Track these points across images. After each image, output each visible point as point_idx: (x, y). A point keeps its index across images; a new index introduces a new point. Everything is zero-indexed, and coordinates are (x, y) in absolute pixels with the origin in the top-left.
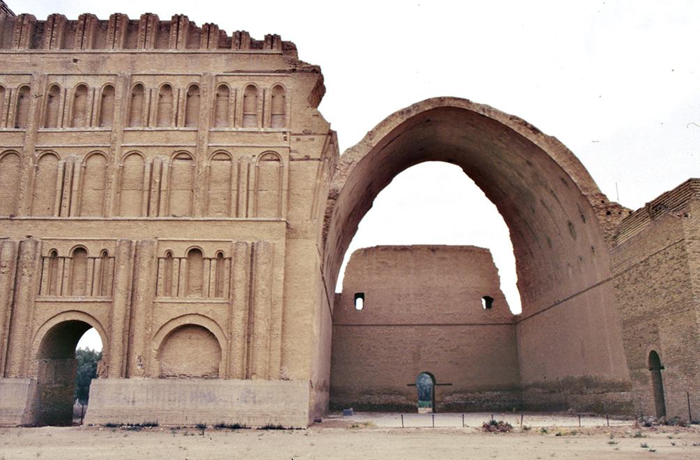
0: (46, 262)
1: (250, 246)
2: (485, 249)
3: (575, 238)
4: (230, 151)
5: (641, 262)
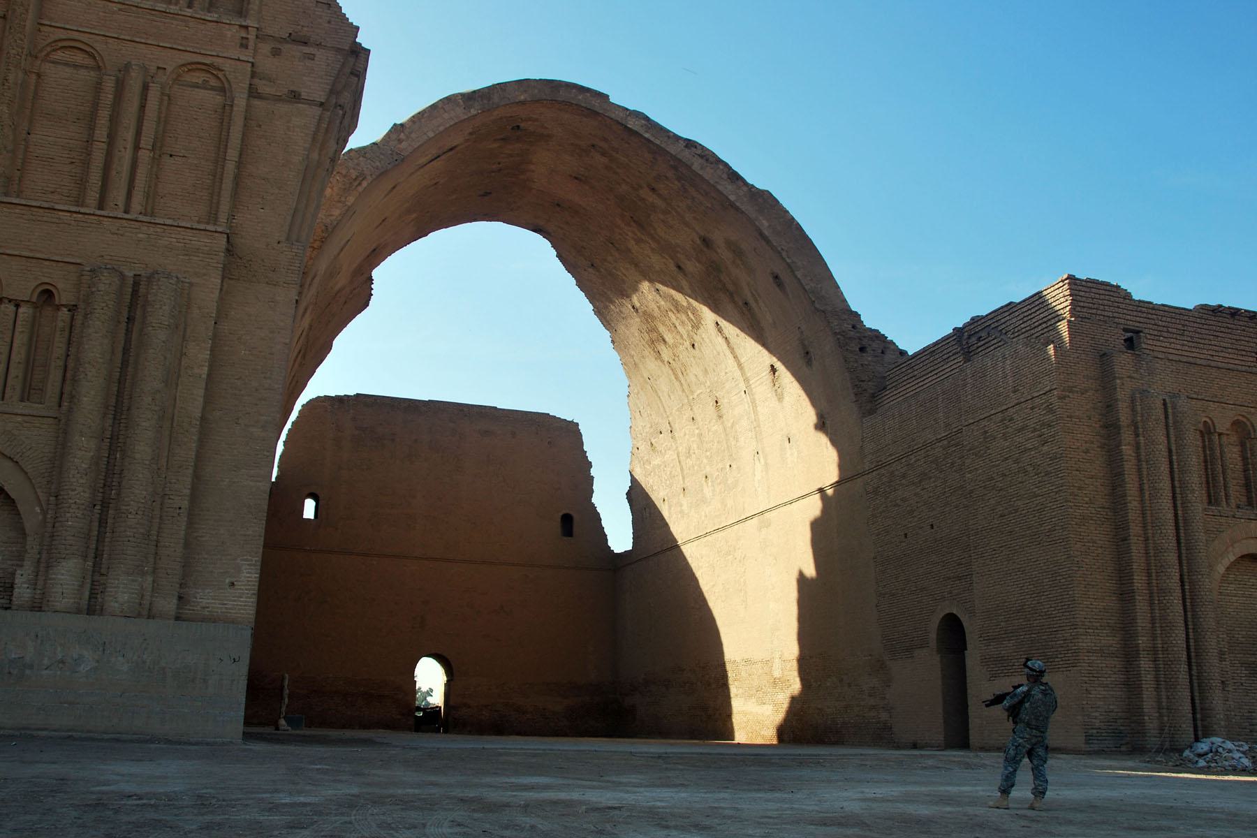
1: (131, 281)
3: (780, 398)
4: (98, 46)
5: (939, 440)
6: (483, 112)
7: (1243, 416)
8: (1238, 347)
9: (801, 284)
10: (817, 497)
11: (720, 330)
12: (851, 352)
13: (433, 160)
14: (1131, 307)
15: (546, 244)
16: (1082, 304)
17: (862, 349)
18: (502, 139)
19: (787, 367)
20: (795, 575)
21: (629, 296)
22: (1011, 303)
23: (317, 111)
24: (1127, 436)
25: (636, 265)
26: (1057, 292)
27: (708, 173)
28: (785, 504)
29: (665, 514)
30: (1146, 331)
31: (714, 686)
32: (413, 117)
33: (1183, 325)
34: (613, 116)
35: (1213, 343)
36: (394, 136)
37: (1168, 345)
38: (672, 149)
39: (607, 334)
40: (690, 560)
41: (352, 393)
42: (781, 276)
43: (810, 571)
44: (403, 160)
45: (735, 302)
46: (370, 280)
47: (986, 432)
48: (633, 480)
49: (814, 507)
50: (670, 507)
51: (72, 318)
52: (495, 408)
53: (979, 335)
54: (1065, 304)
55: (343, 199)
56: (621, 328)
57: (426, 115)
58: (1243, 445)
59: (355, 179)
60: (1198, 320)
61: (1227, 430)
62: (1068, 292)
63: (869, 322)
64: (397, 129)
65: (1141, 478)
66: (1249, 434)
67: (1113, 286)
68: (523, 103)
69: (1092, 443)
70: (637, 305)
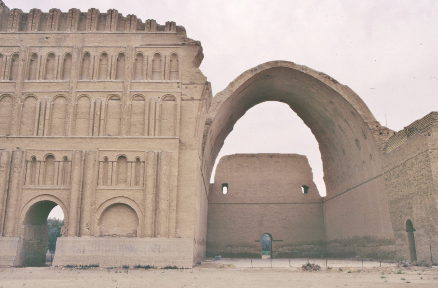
0: (29, 164)
4: (144, 94)
51: (144, 165)
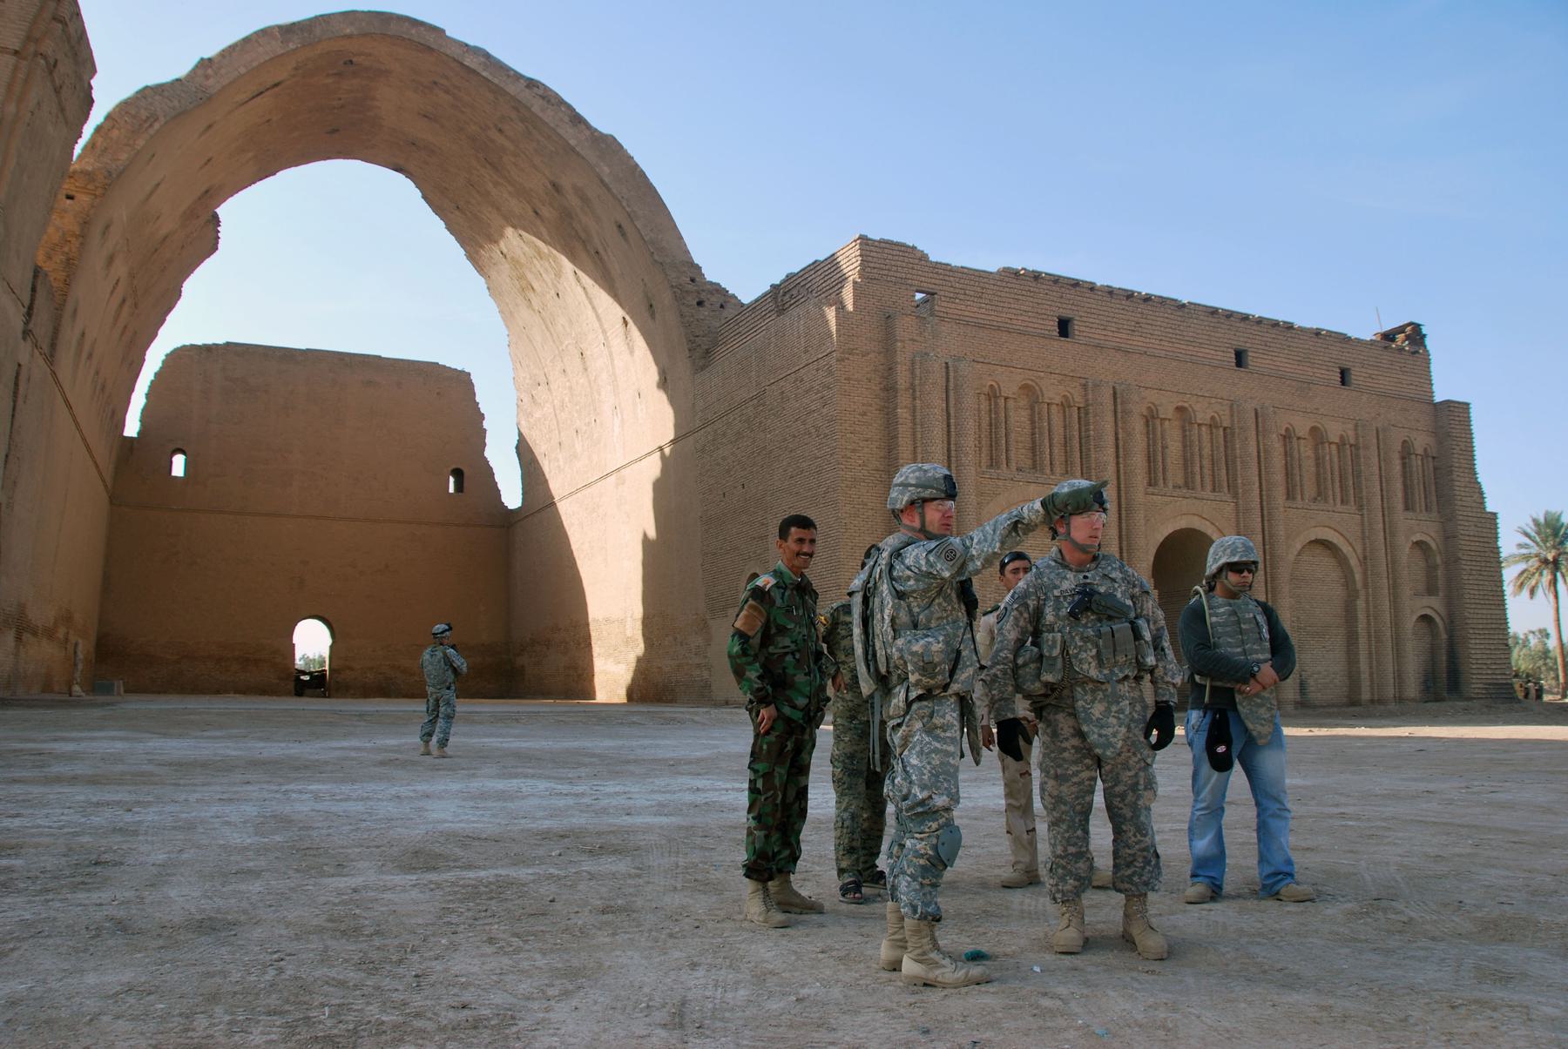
2: (462, 372)
6: (304, 46)
7: (1032, 380)
8: (1039, 311)
9: (640, 233)
10: (658, 454)
11: (578, 280)
12: (688, 306)
13: (253, 98)
14: (927, 269)
15: (409, 184)
16: (872, 265)
17: (700, 303)
18: (336, 74)
19: (635, 324)
20: (640, 538)
21: (496, 242)
22: (816, 261)
23: (11, 60)
24: (903, 399)
25: (498, 209)
26: (851, 251)
27: (548, 116)
28: (636, 461)
29: (546, 469)
30: (942, 293)
31: (582, 645)
32: (223, 51)
33: (983, 288)
34: (448, 52)
35: (1013, 306)
36: (200, 72)
37: (963, 307)
38: (511, 89)
39: (482, 280)
40: (563, 518)
41: (221, 341)
42: (623, 225)
43: (652, 534)
44: (210, 99)
45: (587, 251)
46: (216, 221)
47: (783, 392)
48: (520, 434)
49: (652, 468)
50: (550, 462)
52: (379, 357)
53: (791, 293)
54: (856, 265)
55: (131, 142)
56: (493, 274)
57: (237, 49)
58: (1032, 408)
59: (145, 121)
60: (999, 283)
61: (1014, 394)
62: (858, 253)
63: (711, 274)
64: (205, 64)
65: (915, 441)
66: (1038, 397)
67: (909, 247)
68: (349, 37)
69: (871, 405)
70: (505, 251)
